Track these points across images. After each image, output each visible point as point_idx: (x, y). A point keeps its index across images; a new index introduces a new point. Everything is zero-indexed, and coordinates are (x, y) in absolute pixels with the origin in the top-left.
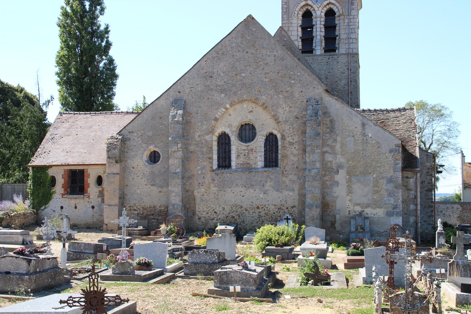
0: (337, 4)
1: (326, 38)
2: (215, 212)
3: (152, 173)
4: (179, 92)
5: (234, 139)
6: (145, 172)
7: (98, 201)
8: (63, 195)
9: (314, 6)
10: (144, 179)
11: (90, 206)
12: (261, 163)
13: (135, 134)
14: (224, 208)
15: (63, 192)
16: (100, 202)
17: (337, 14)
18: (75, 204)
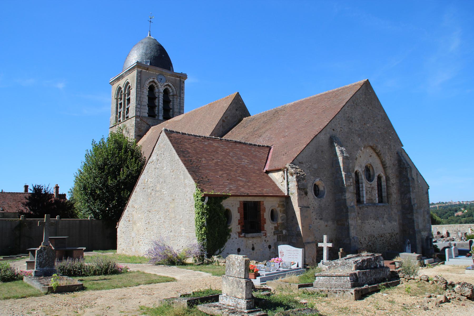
0: (172, 87)
1: (164, 109)
2: (361, 243)
3: (320, 207)
4: (333, 130)
5: (363, 177)
6: (315, 206)
7: (274, 240)
8: (240, 234)
9: (159, 84)
10: (314, 214)
11: (266, 245)
12: (377, 202)
13: (305, 166)
14: (365, 238)
15: (239, 230)
16: (276, 240)
17: (171, 94)
18: (253, 245)
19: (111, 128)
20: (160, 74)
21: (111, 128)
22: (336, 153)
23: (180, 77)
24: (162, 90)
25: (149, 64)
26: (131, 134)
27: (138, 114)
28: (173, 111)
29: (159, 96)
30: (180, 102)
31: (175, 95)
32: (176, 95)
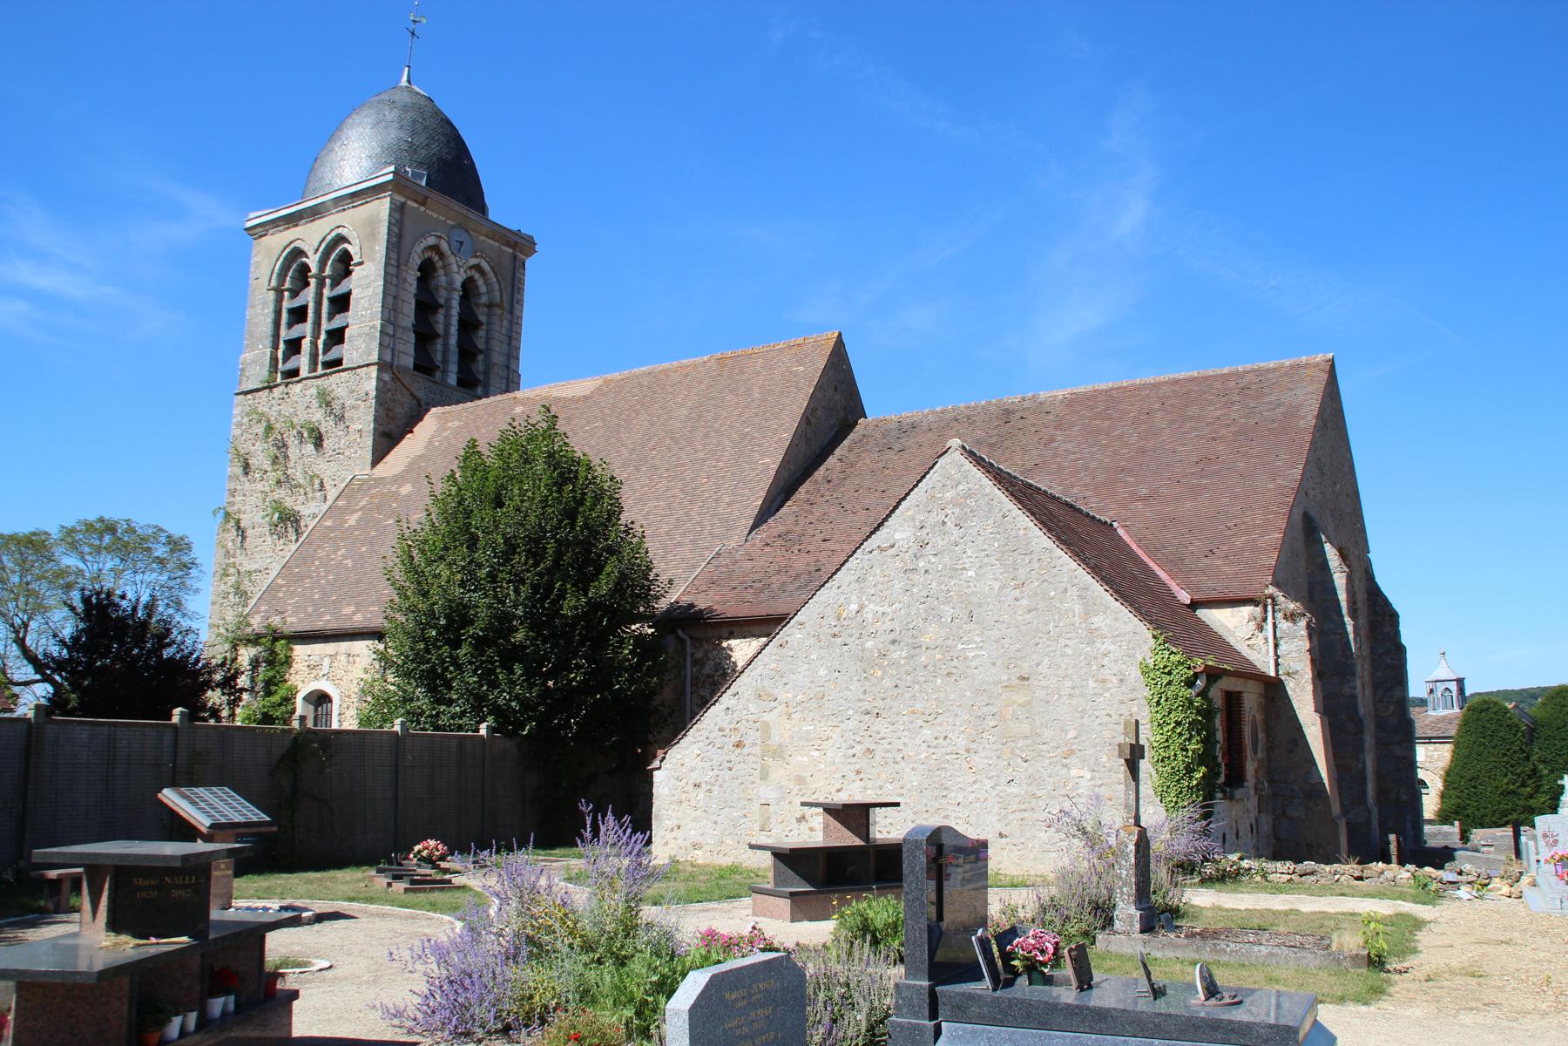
9: (452, 259)
17: (484, 299)
20: (459, 226)
22: (1325, 561)
23: (514, 246)
24: (458, 280)
27: (388, 358)
29: (448, 300)
30: (510, 330)
32: (500, 306)
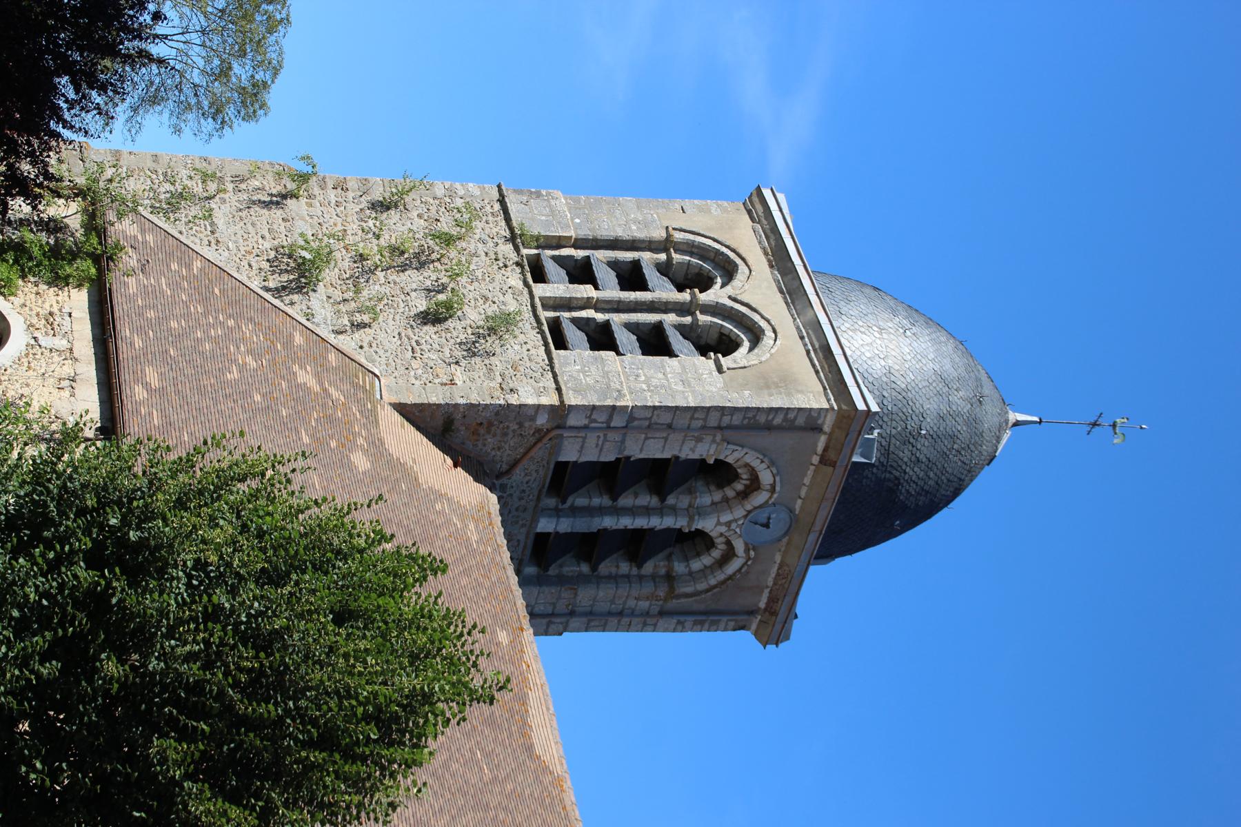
0: (776, 348)
9: (739, 512)
17: (679, 568)
19: (502, 201)
20: (794, 520)
21: (502, 201)
23: (771, 610)
24: (707, 524)
25: (857, 458)
26: (459, 375)
27: (572, 421)
28: (582, 580)
29: (674, 510)
30: (633, 614)
31: (672, 588)
32: (672, 594)
